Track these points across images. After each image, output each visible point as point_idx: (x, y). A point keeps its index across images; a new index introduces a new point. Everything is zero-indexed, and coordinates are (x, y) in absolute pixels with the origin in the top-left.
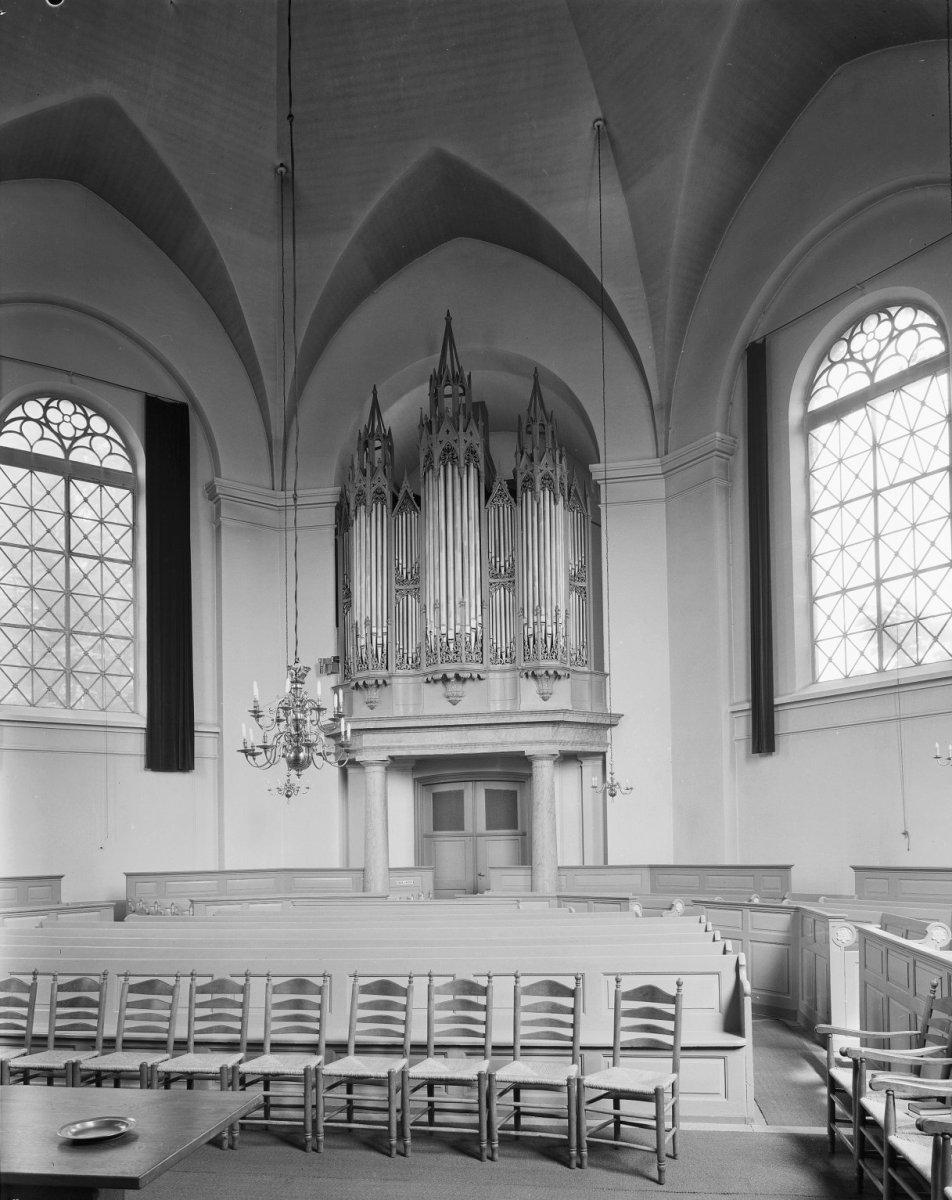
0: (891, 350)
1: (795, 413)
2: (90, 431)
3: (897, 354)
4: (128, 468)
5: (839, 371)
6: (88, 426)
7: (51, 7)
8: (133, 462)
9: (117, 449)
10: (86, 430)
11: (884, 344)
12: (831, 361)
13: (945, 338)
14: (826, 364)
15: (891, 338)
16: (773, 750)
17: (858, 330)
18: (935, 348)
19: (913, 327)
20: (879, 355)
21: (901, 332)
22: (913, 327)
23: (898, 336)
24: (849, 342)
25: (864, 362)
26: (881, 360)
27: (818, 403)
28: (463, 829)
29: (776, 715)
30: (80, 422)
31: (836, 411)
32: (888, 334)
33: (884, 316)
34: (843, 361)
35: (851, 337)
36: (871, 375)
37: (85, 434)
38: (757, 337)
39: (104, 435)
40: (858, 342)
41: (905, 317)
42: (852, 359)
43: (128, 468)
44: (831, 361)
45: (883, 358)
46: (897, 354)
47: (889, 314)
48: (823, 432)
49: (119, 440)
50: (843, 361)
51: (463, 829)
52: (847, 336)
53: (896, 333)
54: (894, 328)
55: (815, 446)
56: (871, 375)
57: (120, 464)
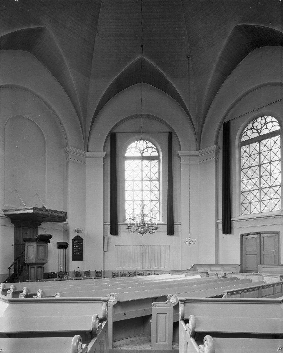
0: (265, 127)
1: (237, 142)
2: (147, 147)
3: (267, 128)
4: (157, 154)
5: (249, 132)
6: (147, 146)
7: (16, 1)
8: (158, 153)
9: (155, 150)
10: (146, 147)
11: (263, 125)
12: (247, 128)
13: (280, 125)
14: (246, 129)
15: (265, 124)
16: (174, 234)
17: (256, 121)
18: (278, 128)
19: (271, 122)
20: (262, 128)
21: (268, 123)
22: (271, 122)
23: (267, 124)
24: (253, 124)
25: (257, 130)
26: (262, 130)
27: (244, 139)
28: (73, 260)
29: (174, 227)
30: (145, 145)
31: (249, 142)
32: (264, 122)
33: (263, 118)
34: (251, 129)
35: (254, 123)
36: (259, 133)
37: (146, 148)
38: (226, 121)
39: (151, 147)
40: (255, 124)
41: (269, 119)
42: (254, 129)
43: (157, 154)
44: (247, 128)
45: (263, 129)
46: (267, 128)
47: (264, 117)
48: (244, 148)
49: (155, 148)
50: (251, 129)
51: (73, 260)
52: (252, 122)
53: (266, 123)
54: (266, 121)
55: (242, 151)
56: (259, 133)
57: (156, 154)
